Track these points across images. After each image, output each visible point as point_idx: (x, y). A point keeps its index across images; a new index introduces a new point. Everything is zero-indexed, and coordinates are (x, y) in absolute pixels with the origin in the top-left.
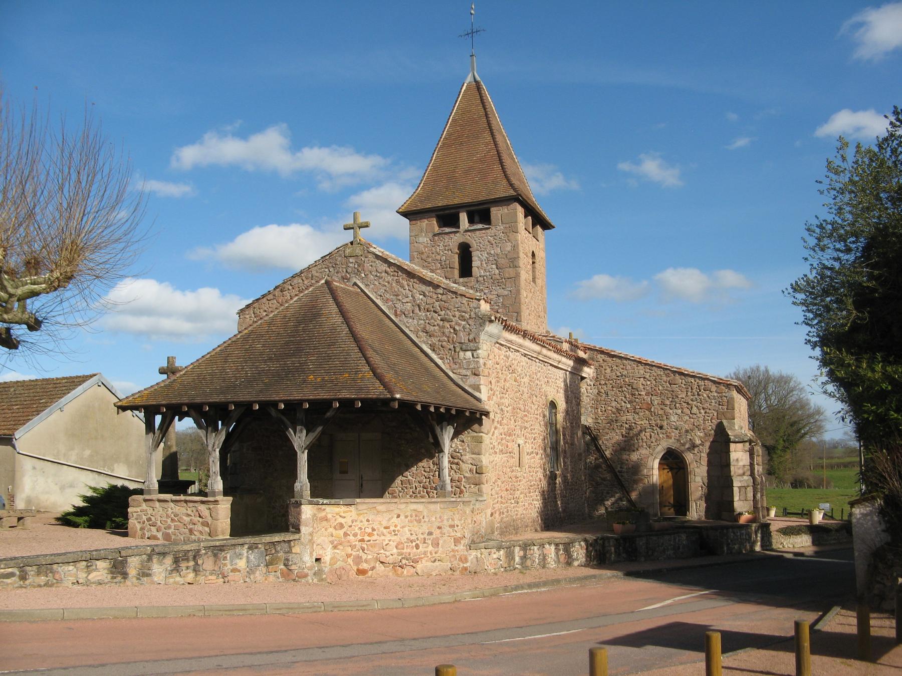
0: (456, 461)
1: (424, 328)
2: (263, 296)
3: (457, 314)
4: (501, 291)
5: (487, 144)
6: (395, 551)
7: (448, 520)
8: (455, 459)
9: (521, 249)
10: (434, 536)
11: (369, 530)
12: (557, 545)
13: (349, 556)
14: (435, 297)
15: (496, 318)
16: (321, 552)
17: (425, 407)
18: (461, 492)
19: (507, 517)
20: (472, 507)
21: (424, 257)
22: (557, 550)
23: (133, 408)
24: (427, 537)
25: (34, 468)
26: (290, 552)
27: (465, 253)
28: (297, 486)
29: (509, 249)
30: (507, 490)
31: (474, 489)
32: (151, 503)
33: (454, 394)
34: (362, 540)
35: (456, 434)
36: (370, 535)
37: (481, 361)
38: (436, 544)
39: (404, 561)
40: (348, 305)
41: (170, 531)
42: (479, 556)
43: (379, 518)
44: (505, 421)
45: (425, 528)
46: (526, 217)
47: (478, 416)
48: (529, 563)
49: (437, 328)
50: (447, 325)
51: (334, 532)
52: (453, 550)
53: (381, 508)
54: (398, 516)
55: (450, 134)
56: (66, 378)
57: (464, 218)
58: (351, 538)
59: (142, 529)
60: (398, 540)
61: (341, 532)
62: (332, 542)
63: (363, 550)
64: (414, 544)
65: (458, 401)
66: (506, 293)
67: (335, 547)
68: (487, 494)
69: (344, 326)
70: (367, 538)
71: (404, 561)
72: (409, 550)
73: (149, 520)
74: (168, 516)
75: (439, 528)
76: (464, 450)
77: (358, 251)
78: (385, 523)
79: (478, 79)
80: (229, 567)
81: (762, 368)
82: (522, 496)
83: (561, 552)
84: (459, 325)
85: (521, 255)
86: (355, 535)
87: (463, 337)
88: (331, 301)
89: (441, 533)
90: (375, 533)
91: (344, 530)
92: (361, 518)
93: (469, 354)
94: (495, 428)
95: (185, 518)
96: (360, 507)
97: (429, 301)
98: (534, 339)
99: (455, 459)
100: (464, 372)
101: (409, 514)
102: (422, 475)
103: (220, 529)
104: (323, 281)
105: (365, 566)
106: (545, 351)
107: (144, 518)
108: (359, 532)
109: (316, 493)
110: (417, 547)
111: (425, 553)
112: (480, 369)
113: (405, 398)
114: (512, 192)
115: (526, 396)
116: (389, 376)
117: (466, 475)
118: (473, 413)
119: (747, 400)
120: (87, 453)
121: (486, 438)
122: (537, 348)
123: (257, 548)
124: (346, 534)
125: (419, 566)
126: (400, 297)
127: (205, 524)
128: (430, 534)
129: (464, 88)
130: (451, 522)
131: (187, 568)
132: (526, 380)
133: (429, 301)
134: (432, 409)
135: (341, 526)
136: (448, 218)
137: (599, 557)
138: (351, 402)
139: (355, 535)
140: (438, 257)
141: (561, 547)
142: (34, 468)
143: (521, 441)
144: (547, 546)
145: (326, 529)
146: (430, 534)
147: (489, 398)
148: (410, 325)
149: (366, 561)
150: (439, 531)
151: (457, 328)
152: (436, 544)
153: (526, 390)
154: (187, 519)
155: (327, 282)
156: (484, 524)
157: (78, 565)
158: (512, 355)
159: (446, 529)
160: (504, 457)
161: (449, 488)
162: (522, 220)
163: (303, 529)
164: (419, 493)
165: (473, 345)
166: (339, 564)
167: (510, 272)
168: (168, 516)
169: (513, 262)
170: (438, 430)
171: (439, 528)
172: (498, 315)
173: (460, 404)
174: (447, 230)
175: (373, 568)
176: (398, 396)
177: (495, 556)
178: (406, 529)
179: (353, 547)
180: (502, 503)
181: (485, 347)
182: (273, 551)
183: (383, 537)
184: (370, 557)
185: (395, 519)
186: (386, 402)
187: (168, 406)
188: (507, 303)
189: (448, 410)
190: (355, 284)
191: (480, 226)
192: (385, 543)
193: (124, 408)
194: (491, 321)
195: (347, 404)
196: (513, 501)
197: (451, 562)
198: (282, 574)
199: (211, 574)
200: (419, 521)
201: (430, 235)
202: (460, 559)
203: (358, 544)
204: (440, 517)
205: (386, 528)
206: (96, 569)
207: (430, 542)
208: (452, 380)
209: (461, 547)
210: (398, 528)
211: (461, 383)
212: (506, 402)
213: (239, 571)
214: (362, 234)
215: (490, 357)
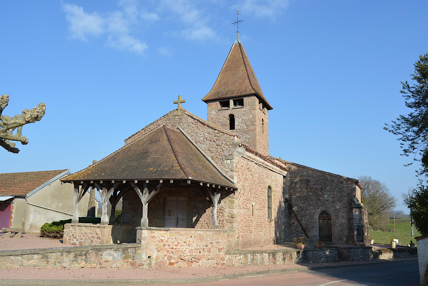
0: (221, 211)
1: (209, 149)
2: (137, 133)
3: (224, 142)
4: (247, 136)
5: (243, 71)
6: (189, 254)
7: (216, 240)
8: (221, 211)
9: (257, 117)
10: (209, 247)
11: (176, 243)
12: (269, 254)
13: (165, 256)
14: (214, 134)
15: (242, 145)
16: (151, 254)
17: (205, 184)
18: (224, 226)
19: (246, 239)
20: (228, 233)
21: (214, 120)
22: (269, 255)
23: (69, 182)
24: (205, 248)
25: (35, 211)
26: (135, 253)
27: (232, 118)
28: (142, 220)
29: (251, 117)
30: (246, 226)
31: (230, 225)
32: (74, 227)
33: (220, 179)
34: (172, 248)
35: (222, 198)
36: (176, 246)
37: (234, 165)
38: (209, 251)
39: (193, 259)
40: (172, 136)
41: (82, 241)
42: (231, 258)
43: (181, 237)
44: (246, 194)
45: (204, 243)
46: (259, 103)
47: (232, 190)
48: (255, 262)
49: (214, 149)
50: (219, 147)
51: (158, 244)
52: (218, 255)
53: (183, 232)
54: (191, 237)
55: (227, 67)
56: (54, 171)
57: (231, 102)
58: (167, 247)
59: (69, 239)
60: (190, 248)
61: (162, 244)
62: (157, 249)
63: (173, 253)
64: (198, 251)
65: (224, 183)
66: (250, 137)
67: (158, 251)
68: (236, 228)
69: (169, 146)
70: (174, 247)
71: (193, 259)
72: (196, 254)
73: (73, 235)
74: (82, 234)
75: (211, 243)
76: (225, 206)
77: (179, 113)
78: (184, 240)
79: (240, 42)
80: (103, 259)
81: (368, 178)
82: (253, 229)
83: (271, 257)
84: (225, 147)
85: (257, 120)
86: (169, 245)
87: (226, 153)
88: (165, 134)
89: (212, 246)
90: (179, 245)
91: (163, 243)
92: (172, 237)
93: (229, 161)
94: (241, 197)
95: (89, 235)
96: (172, 232)
97: (211, 136)
98: (260, 156)
99: (221, 211)
100: (226, 170)
101: (196, 236)
102: (206, 218)
103: (105, 241)
104: (162, 126)
105: (173, 261)
106: (266, 162)
107: (71, 234)
108: (171, 244)
109: (152, 223)
110: (200, 252)
111: (204, 255)
112: (234, 169)
113: (194, 179)
114: (253, 92)
115: (256, 182)
116: (187, 169)
117: (226, 218)
118: (229, 189)
119: (361, 189)
120: (61, 204)
121: (236, 201)
122: (262, 161)
123: (118, 250)
124: (164, 245)
125: (200, 262)
126: (198, 135)
127: (99, 238)
128: (207, 246)
129: (233, 46)
130: (217, 241)
131: (82, 260)
132: (257, 175)
133: (211, 136)
134: (208, 185)
135: (162, 241)
136: (225, 103)
137: (305, 259)
138: (169, 180)
139: (169, 245)
140: (220, 121)
141: (271, 255)
142: (35, 211)
143: (253, 204)
144: (264, 254)
145: (154, 242)
146: (207, 246)
147: (238, 183)
148: (202, 147)
149: (174, 258)
150: (211, 245)
151: (224, 149)
152: (209, 251)
153: (256, 180)
154: (91, 235)
155: (163, 126)
156: (234, 242)
157: (23, 256)
158: (250, 163)
159: (215, 244)
160: (245, 211)
161: (217, 224)
162: (258, 105)
163: (143, 242)
164: (204, 226)
165: (230, 157)
166: (160, 259)
167: (251, 128)
168: (82, 234)
169: (253, 123)
170: (212, 196)
171: (211, 243)
172: (243, 144)
173: (223, 184)
174: (224, 108)
175: (177, 262)
176: (190, 178)
177: (238, 258)
178: (195, 243)
179: (168, 252)
180: (243, 232)
181: (236, 159)
182: (127, 252)
183: (183, 247)
184: (176, 256)
185: (189, 239)
186: (185, 181)
187: (85, 181)
188: (250, 141)
189: (217, 186)
190: (178, 128)
191: (239, 107)
192: (184, 250)
193: (65, 182)
194: (240, 146)
195: (166, 181)
196: (249, 232)
197: (216, 260)
198: (131, 264)
199: (94, 263)
200: (201, 240)
201: (217, 110)
202: (221, 259)
203: (171, 250)
204: (212, 238)
205: (184, 242)
206: (33, 259)
207: (206, 250)
208: (221, 173)
209: (222, 253)
210: (191, 242)
211: (225, 175)
212: (247, 185)
213: (109, 262)
214: (182, 106)
215: (239, 163)
